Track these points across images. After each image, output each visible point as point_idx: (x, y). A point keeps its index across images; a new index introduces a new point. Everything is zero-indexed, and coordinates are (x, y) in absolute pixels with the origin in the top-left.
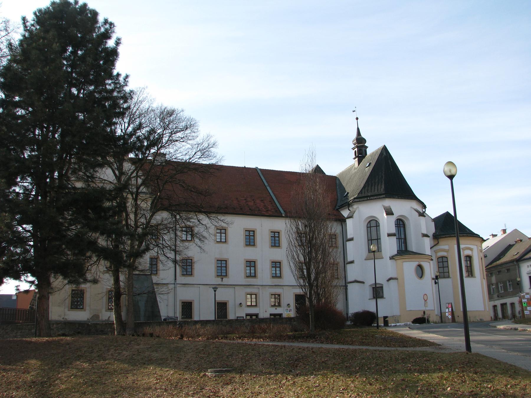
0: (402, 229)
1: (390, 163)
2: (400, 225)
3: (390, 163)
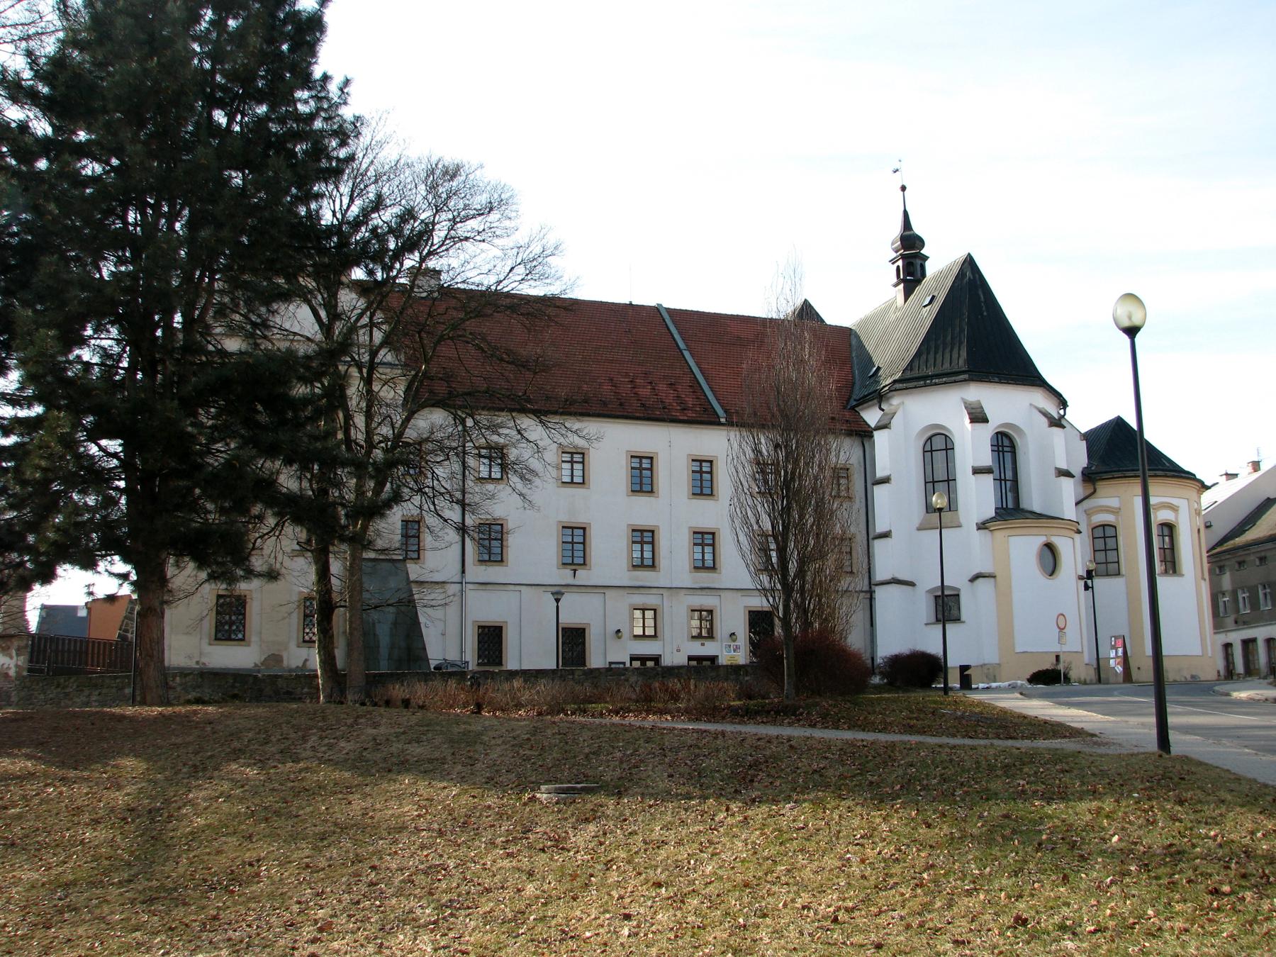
0: (1008, 456)
2: (1003, 446)
3: (982, 296)
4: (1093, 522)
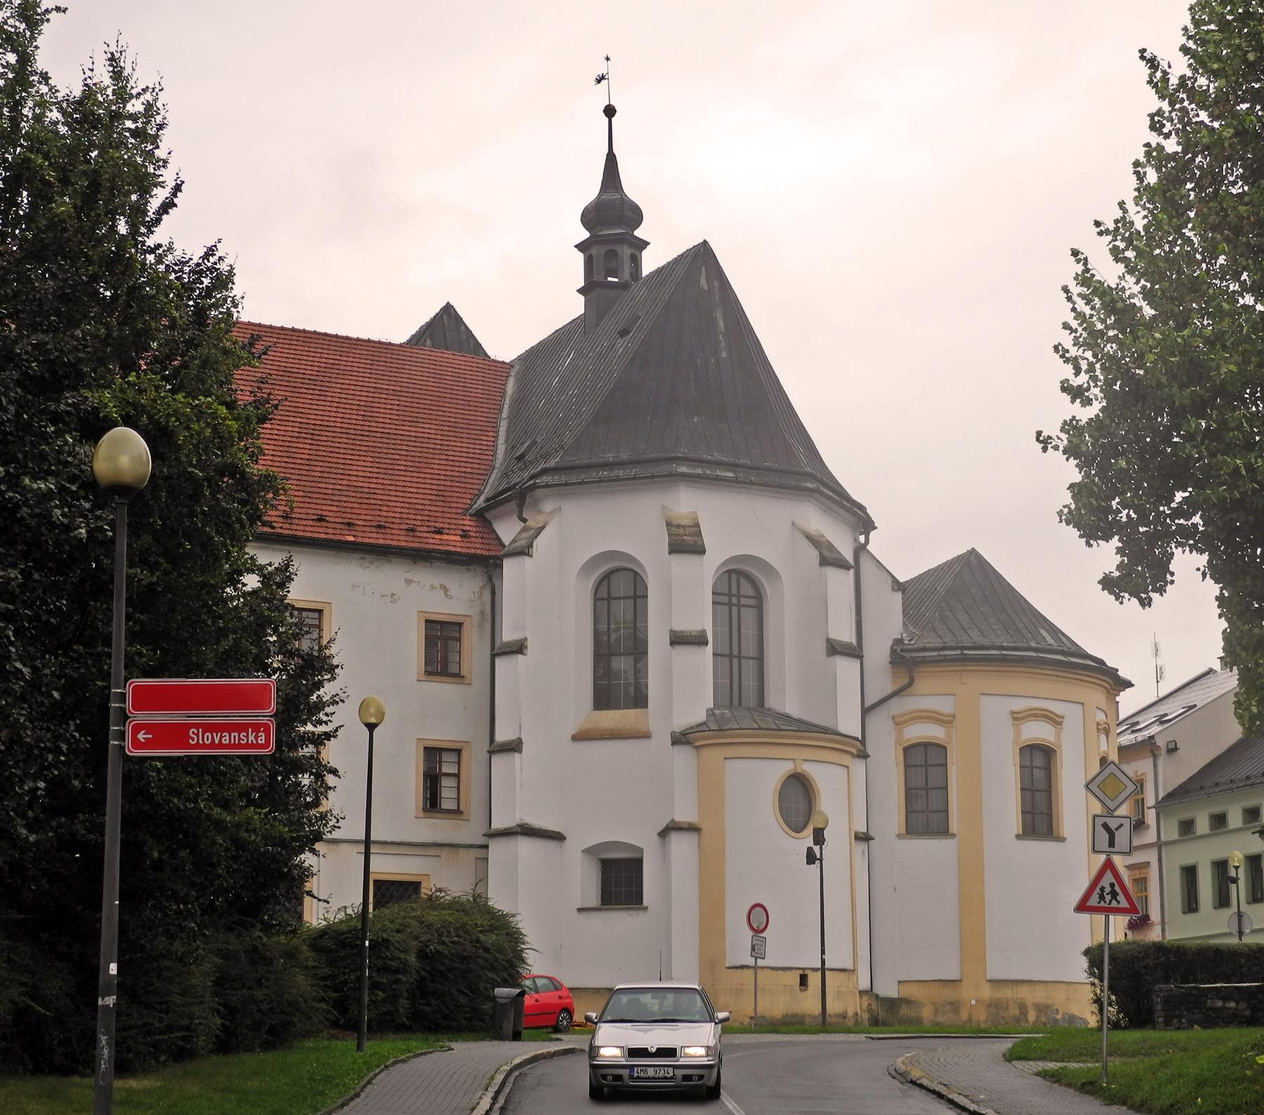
0: (749, 615)
1: (721, 323)
2: (739, 596)
3: (721, 323)
4: (906, 737)
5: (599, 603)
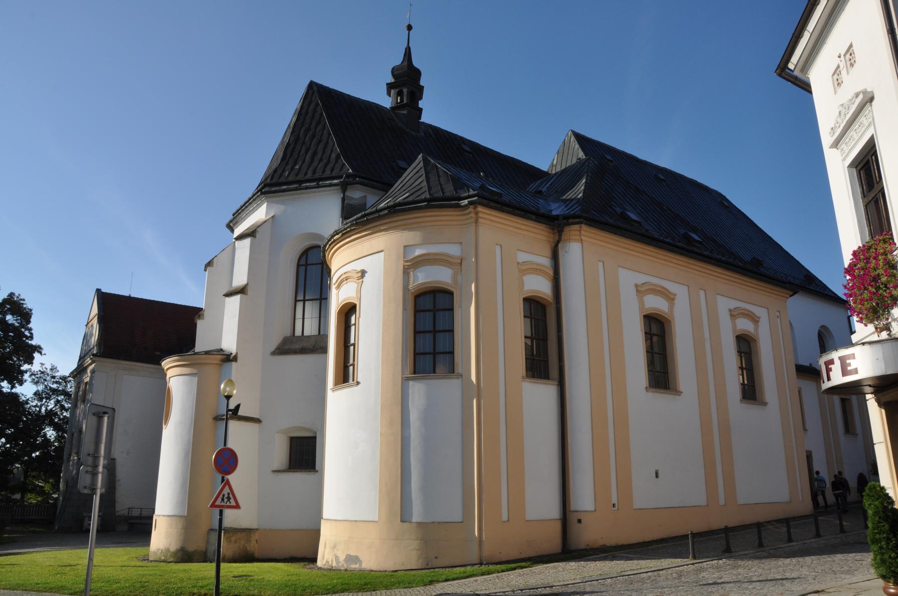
5: (301, 267)
